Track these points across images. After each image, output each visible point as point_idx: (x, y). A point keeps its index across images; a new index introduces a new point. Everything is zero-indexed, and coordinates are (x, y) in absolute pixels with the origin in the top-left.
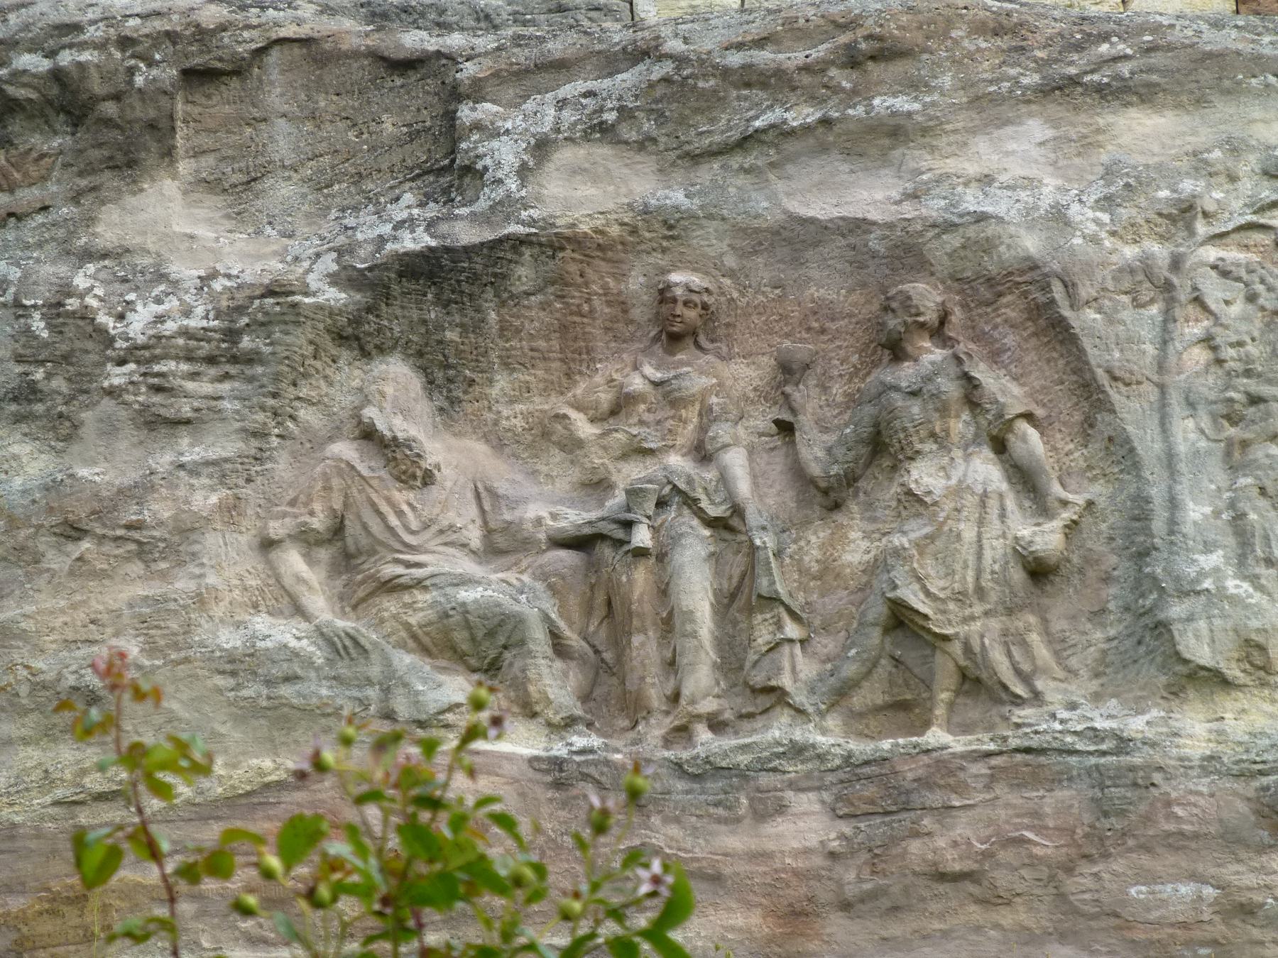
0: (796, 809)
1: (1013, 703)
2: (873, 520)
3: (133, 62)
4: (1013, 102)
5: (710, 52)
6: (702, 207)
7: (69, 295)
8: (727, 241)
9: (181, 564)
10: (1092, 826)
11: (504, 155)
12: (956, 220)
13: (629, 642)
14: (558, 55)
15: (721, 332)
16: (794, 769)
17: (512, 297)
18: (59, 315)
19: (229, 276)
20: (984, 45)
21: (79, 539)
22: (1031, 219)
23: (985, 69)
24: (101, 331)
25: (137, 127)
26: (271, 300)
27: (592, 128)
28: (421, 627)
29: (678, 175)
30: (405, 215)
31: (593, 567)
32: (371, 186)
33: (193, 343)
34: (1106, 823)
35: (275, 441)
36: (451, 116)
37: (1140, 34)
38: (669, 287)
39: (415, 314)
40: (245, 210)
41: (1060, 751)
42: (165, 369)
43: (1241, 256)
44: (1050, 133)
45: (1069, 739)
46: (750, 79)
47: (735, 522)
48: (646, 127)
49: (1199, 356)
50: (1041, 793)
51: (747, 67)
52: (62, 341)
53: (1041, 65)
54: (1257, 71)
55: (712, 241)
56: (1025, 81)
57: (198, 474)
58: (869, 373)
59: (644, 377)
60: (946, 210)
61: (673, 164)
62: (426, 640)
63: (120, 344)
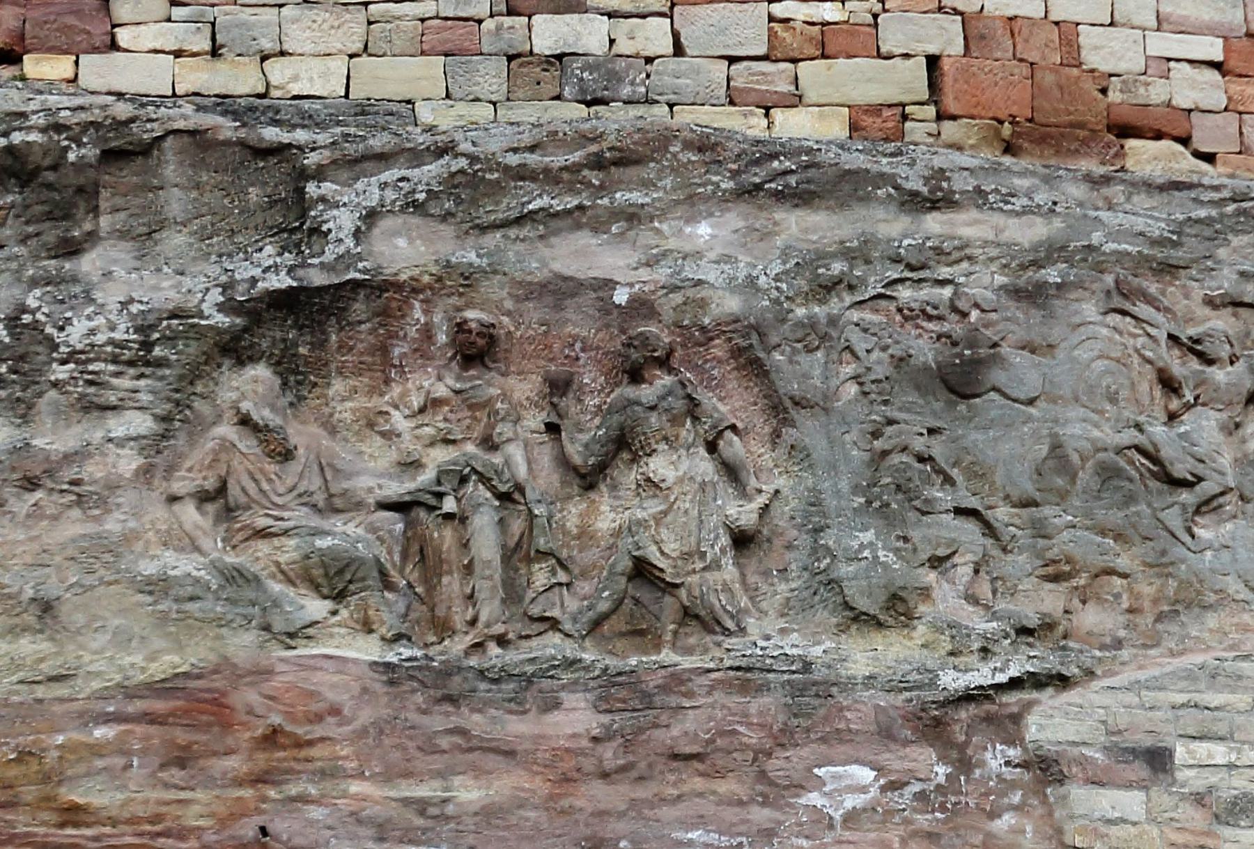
0: (566, 705)
1: (723, 634)
2: (617, 498)
3: (66, 143)
4: (715, 200)
5: (493, 154)
6: (489, 265)
7: (24, 311)
8: (506, 290)
9: (109, 511)
10: (785, 724)
11: (342, 222)
12: (680, 284)
13: (440, 582)
14: (379, 150)
15: (499, 355)
16: (566, 677)
17: (349, 324)
18: (16, 326)
19: (141, 302)
20: (693, 158)
21: (33, 490)
22: (731, 285)
23: (696, 176)
24: (50, 339)
25: (70, 191)
26: (175, 322)
27: (408, 204)
28: (287, 564)
29: (471, 241)
30: (271, 262)
31: (409, 525)
32: (241, 239)
33: (117, 350)
34: (795, 722)
35: (177, 424)
36: (301, 192)
37: (800, 154)
38: (466, 321)
39: (278, 335)
40: (147, 254)
41: (762, 670)
42: (97, 369)
43: (875, 318)
44: (741, 224)
45: (768, 661)
46: (522, 174)
47: (517, 496)
48: (447, 206)
49: (853, 389)
50: (748, 699)
51: (523, 165)
52: (19, 346)
53: (735, 174)
54: (881, 184)
55: (495, 289)
56: (723, 186)
57: (123, 447)
58: (612, 391)
59: (447, 386)
60: (671, 276)
61: (467, 233)
62: (291, 574)
63: (63, 349)
